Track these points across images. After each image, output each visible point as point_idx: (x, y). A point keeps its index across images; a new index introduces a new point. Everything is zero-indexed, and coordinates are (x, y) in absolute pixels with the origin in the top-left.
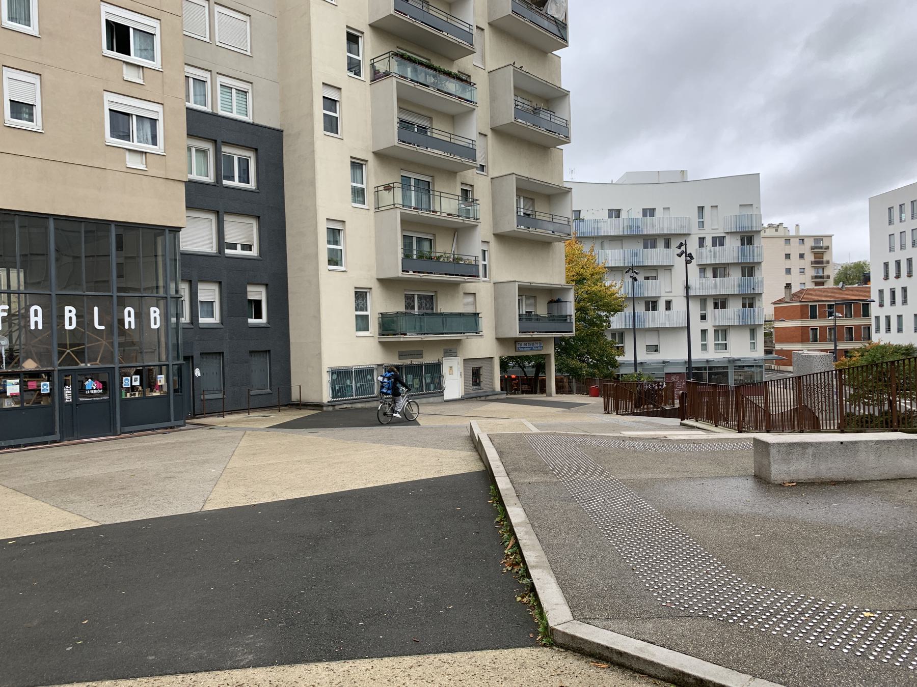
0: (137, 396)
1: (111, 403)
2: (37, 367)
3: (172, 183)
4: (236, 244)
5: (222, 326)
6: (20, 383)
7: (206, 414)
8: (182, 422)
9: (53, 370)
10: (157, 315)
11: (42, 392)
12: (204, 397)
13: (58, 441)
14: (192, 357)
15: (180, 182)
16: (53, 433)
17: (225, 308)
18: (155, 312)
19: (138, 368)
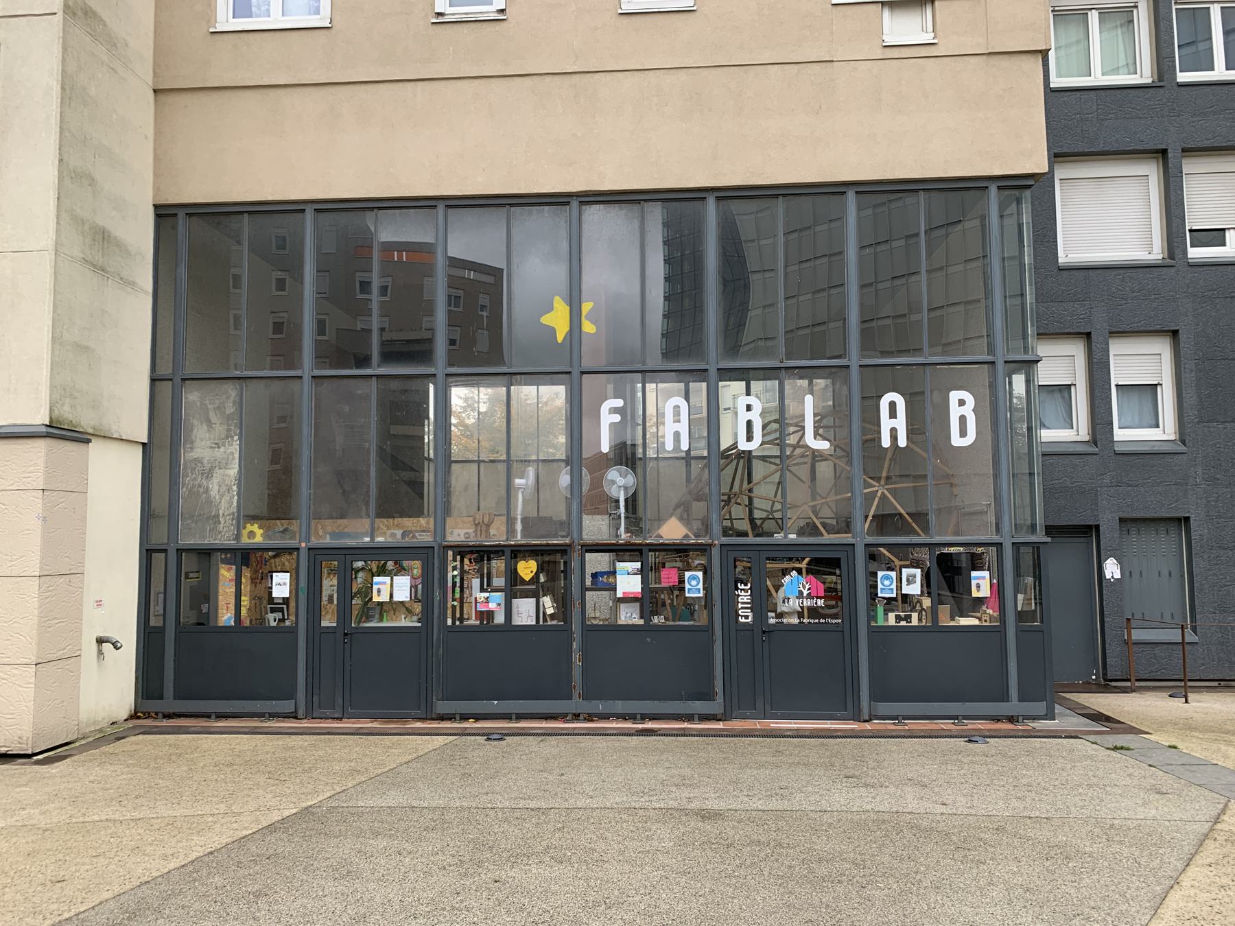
0: (915, 621)
1: (566, 630)
2: (686, 536)
3: (1005, 62)
4: (1224, 230)
5: (1183, 448)
6: (641, 571)
7: (1137, 680)
8: (1040, 708)
9: (710, 545)
10: (968, 411)
11: (687, 595)
12: (1129, 635)
13: (719, 717)
14: (1097, 527)
15: (1029, 56)
16: (708, 696)
17: (1191, 398)
18: (962, 403)
19: (946, 551)
